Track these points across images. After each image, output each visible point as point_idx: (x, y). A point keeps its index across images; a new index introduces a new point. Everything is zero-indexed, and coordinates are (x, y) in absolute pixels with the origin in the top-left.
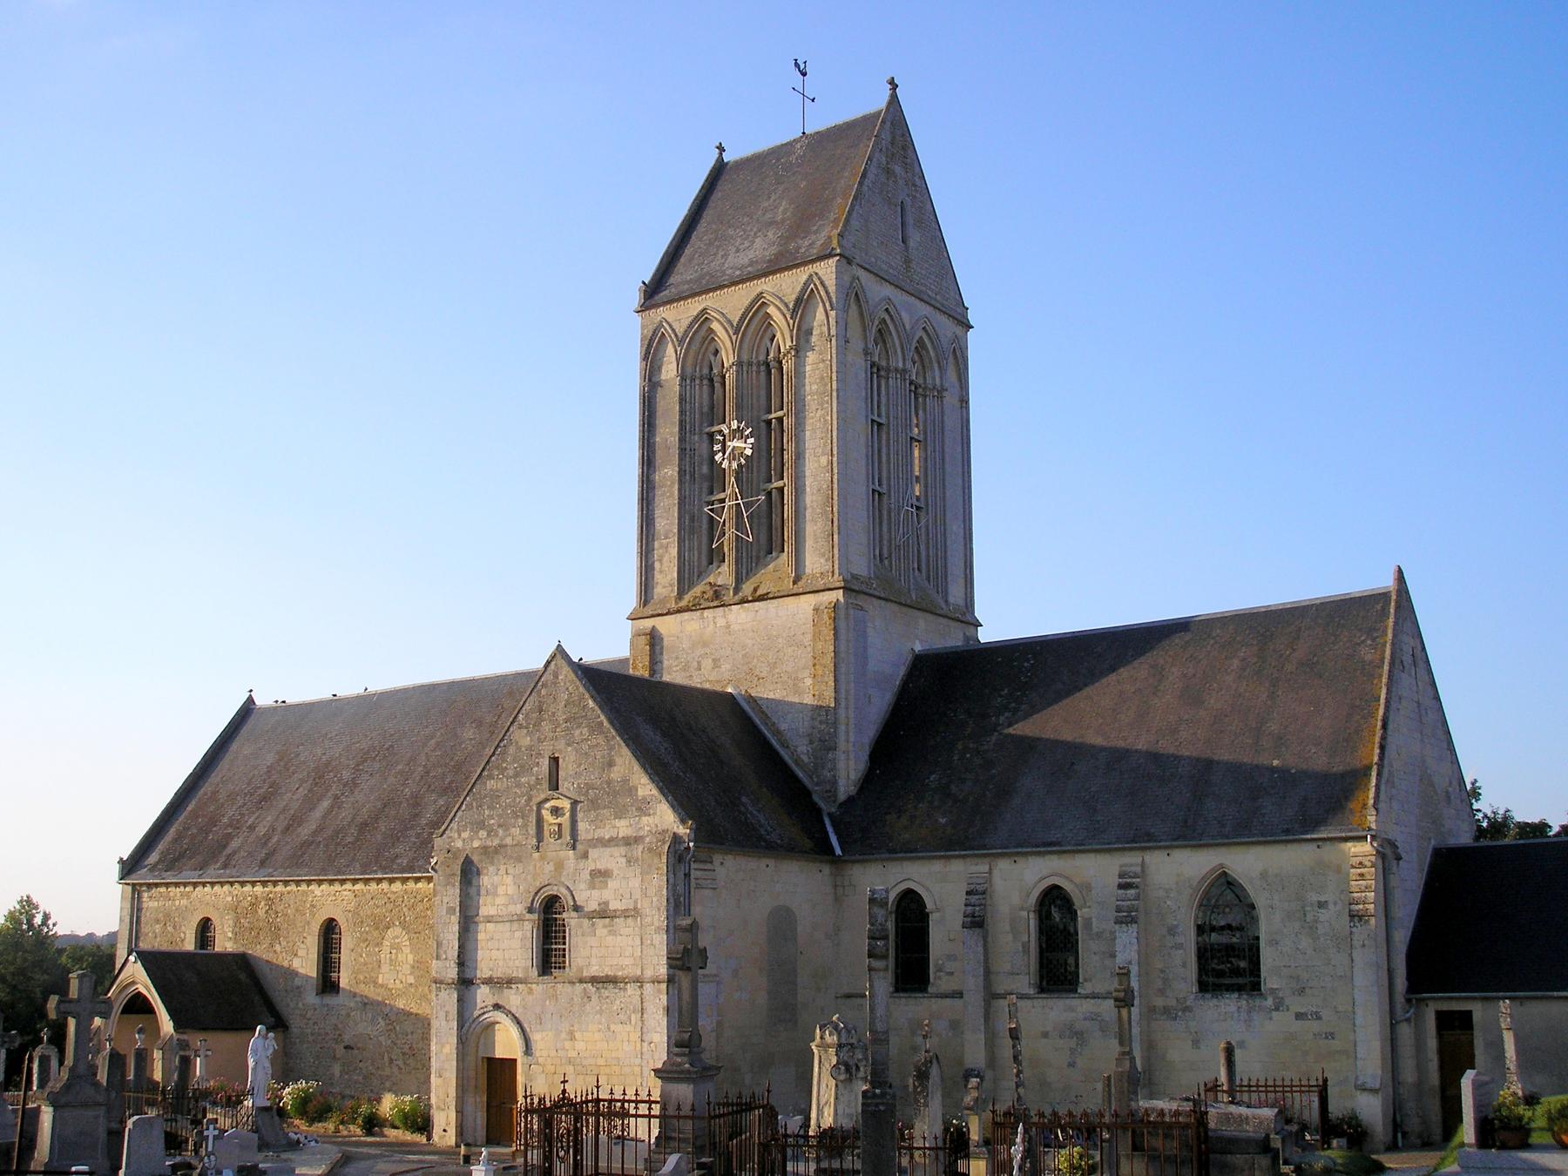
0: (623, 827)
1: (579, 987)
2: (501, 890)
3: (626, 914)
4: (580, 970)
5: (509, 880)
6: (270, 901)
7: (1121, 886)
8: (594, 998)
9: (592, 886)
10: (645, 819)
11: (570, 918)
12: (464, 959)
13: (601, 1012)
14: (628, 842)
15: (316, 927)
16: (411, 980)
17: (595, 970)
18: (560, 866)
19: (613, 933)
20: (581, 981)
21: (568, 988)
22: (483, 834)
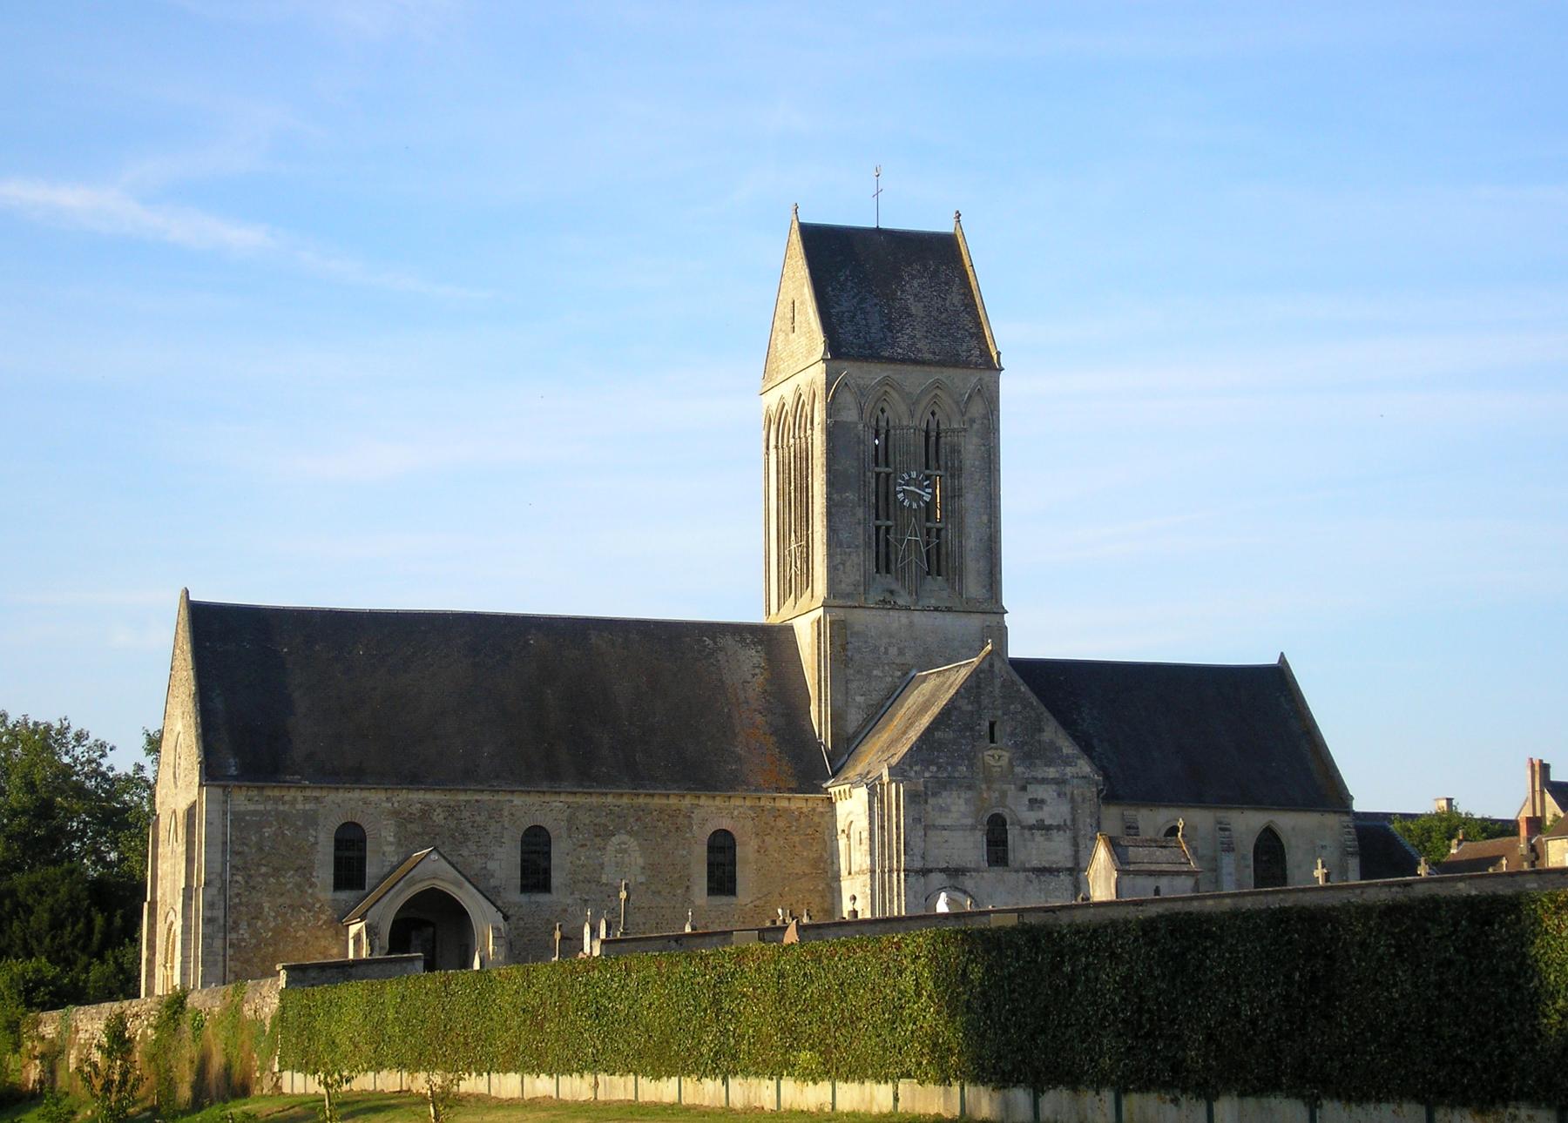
0: (1052, 772)
1: (1022, 875)
2: (954, 808)
3: (1059, 828)
4: (1023, 863)
5: (961, 801)
6: (451, 811)
7: (888, 571)
8: (1035, 882)
9: (1031, 809)
10: (1068, 769)
11: (1013, 834)
12: (931, 871)
13: (1040, 890)
14: (1055, 781)
15: (701, 852)
16: (642, 879)
17: (1035, 863)
18: (1004, 794)
19: (1049, 840)
20: (1025, 870)
21: (1014, 875)
22: (934, 768)
